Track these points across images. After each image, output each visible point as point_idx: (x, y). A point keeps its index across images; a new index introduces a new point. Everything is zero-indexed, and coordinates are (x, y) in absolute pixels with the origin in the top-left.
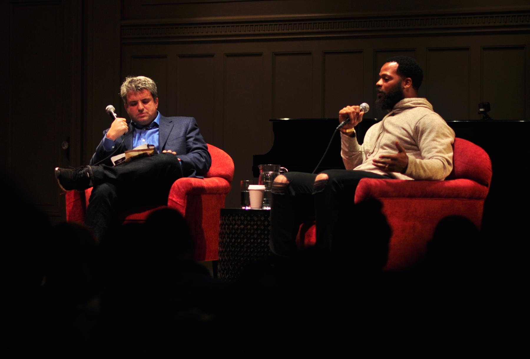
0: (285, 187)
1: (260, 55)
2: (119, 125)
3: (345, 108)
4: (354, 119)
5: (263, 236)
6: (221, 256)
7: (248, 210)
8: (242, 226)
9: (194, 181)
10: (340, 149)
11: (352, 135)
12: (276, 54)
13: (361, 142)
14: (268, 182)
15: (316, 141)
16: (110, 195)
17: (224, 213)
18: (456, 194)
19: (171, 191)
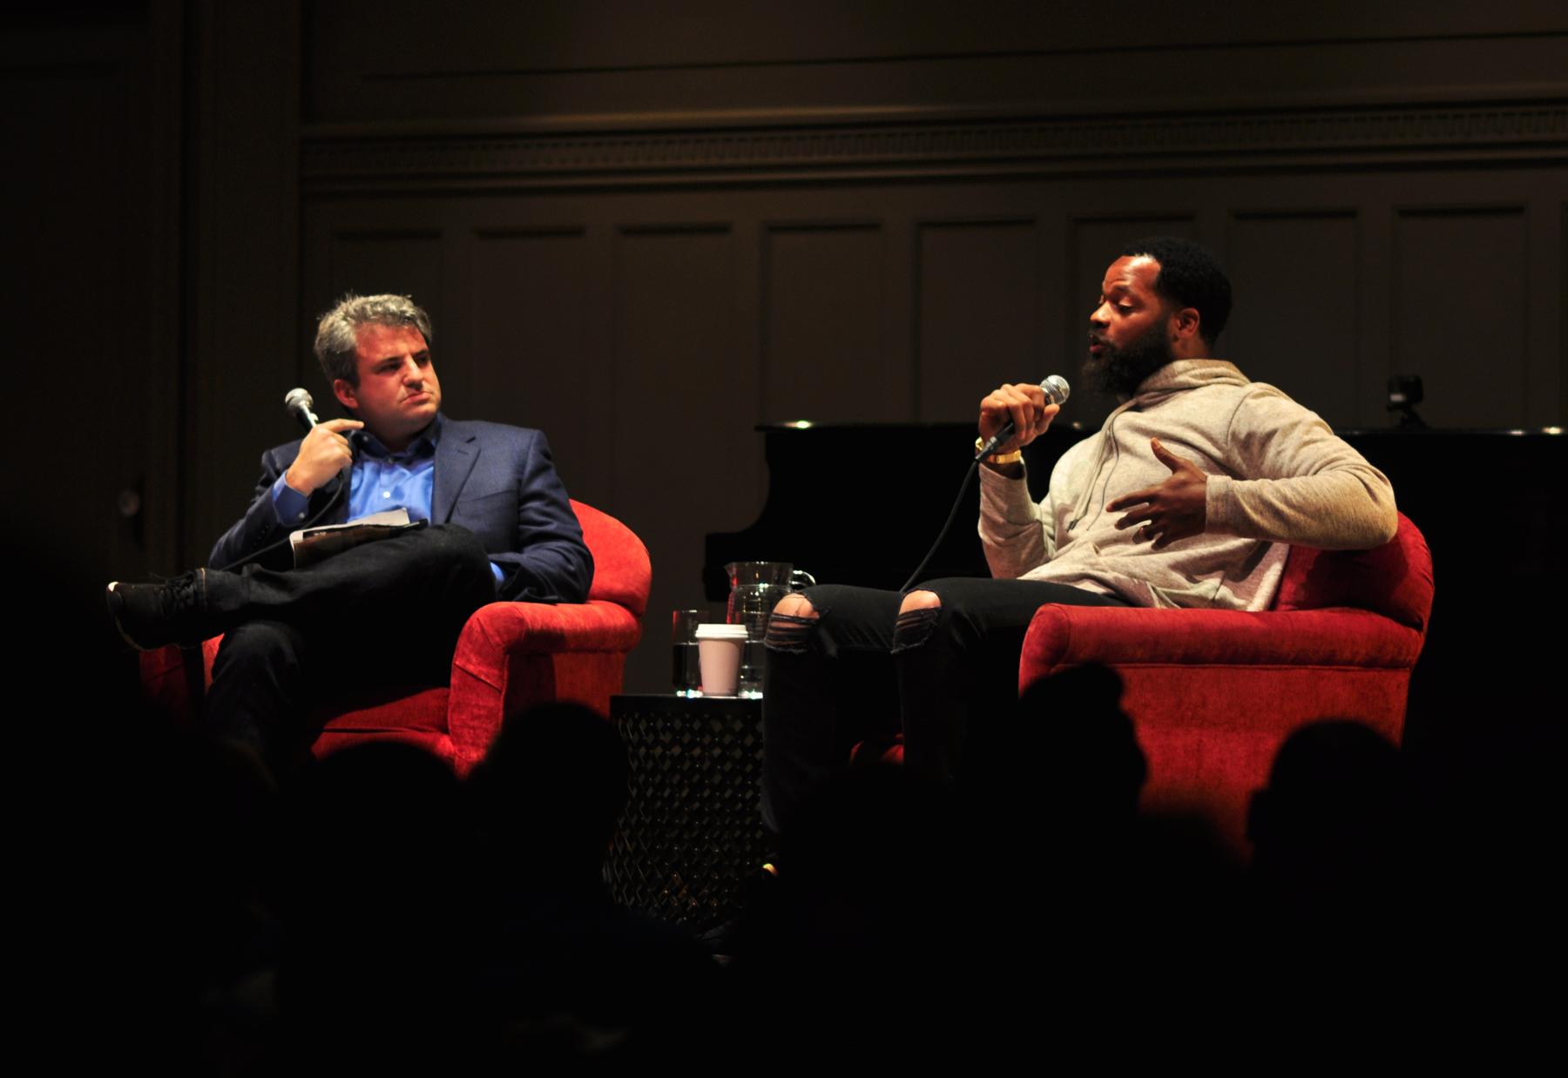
0: (806, 630)
1: (722, 229)
2: (324, 445)
3: (996, 392)
4: (1028, 428)
5: (738, 781)
7: (695, 700)
8: (677, 750)
9: (534, 613)
10: (976, 513)
11: (1013, 472)
12: (775, 229)
13: (1040, 490)
15: (907, 491)
16: (277, 653)
19: (462, 643)
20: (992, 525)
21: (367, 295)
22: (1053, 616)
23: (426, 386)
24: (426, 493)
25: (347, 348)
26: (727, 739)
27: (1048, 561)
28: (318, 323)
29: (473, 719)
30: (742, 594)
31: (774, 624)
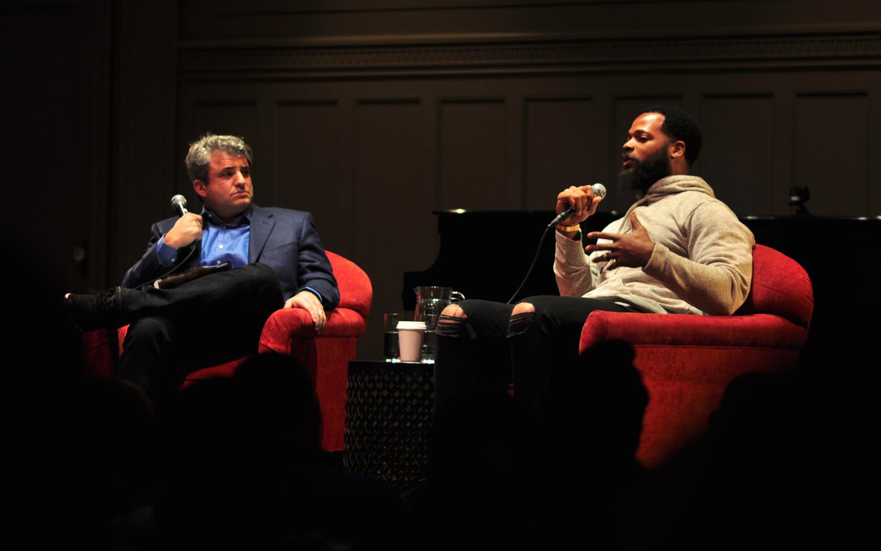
0: (460, 324)
1: (414, 101)
3: (567, 190)
5: (420, 410)
6: (348, 442)
7: (397, 364)
8: (385, 393)
12: (445, 101)
15: (509, 248)
17: (355, 368)
19: (265, 330)
20: (562, 266)
21: (218, 135)
22: (598, 317)
23: (247, 189)
24: (245, 246)
25: (205, 163)
26: (414, 386)
27: (594, 288)
30: (423, 304)
31: (441, 321)
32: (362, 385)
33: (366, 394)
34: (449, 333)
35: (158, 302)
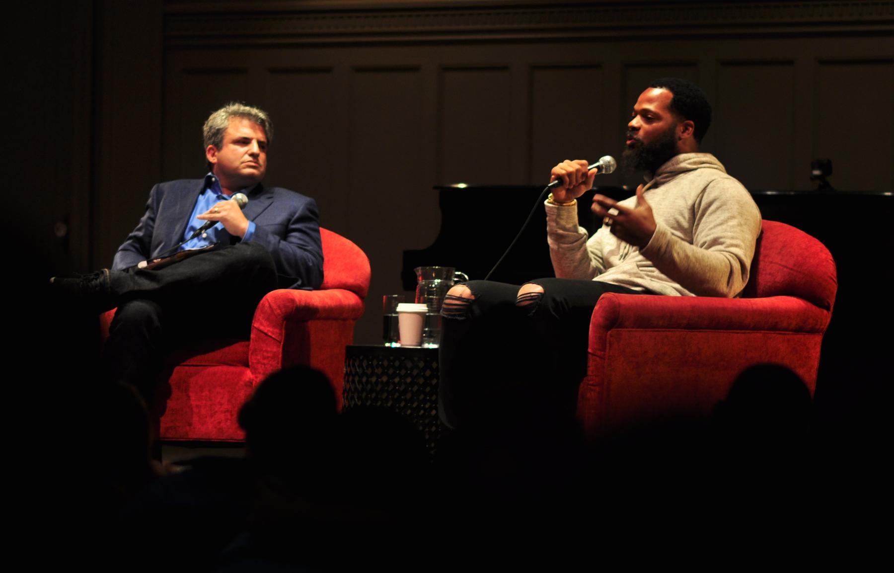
0: (467, 305)
1: (414, 69)
3: (561, 164)
5: (422, 397)
7: (396, 348)
8: (385, 379)
14: (436, 298)
15: (501, 229)
17: (352, 353)
18: (770, 323)
26: (415, 372)
28: (210, 114)
29: (264, 358)
31: (447, 301)
32: (359, 370)
33: (364, 379)
34: (455, 315)
35: (147, 284)
